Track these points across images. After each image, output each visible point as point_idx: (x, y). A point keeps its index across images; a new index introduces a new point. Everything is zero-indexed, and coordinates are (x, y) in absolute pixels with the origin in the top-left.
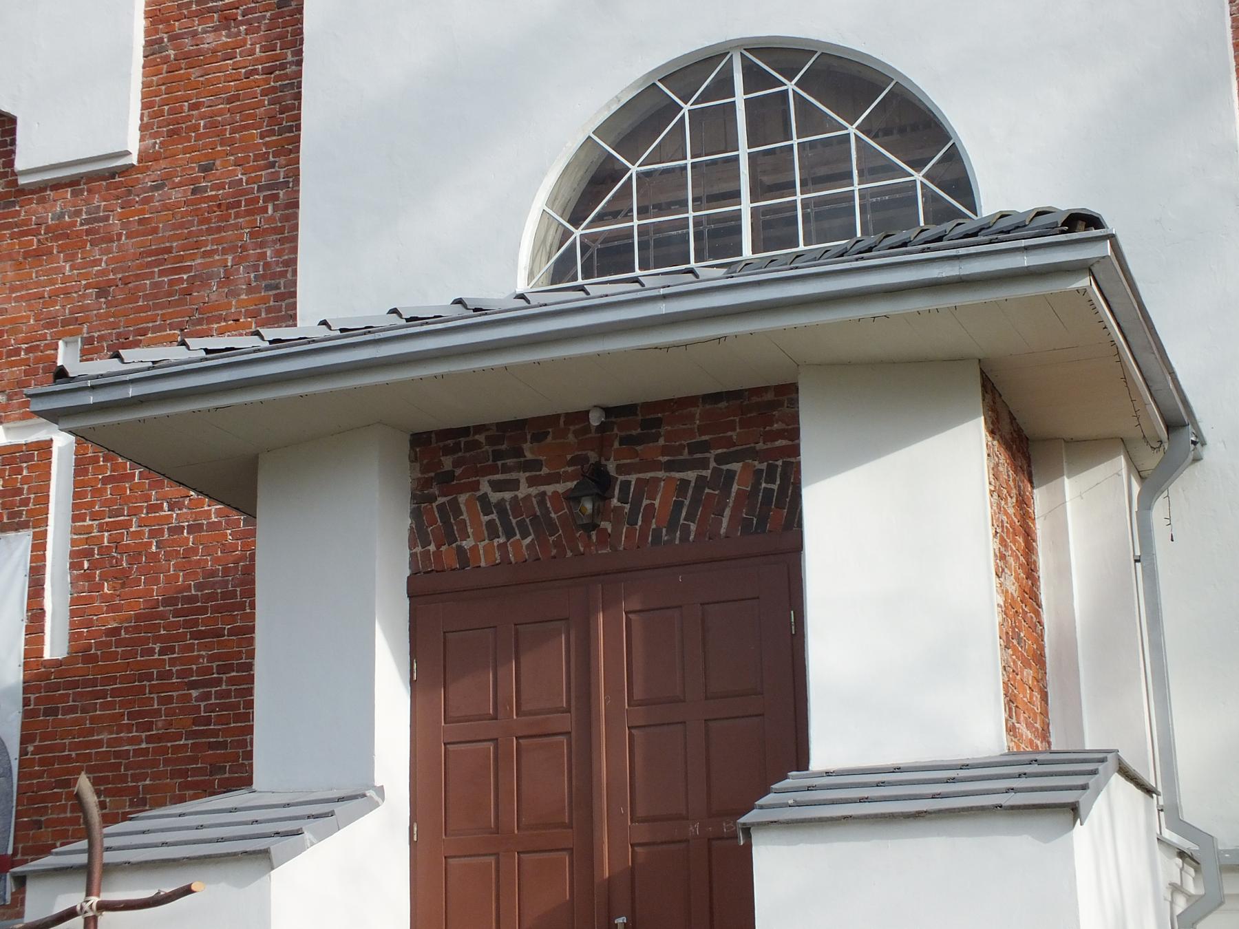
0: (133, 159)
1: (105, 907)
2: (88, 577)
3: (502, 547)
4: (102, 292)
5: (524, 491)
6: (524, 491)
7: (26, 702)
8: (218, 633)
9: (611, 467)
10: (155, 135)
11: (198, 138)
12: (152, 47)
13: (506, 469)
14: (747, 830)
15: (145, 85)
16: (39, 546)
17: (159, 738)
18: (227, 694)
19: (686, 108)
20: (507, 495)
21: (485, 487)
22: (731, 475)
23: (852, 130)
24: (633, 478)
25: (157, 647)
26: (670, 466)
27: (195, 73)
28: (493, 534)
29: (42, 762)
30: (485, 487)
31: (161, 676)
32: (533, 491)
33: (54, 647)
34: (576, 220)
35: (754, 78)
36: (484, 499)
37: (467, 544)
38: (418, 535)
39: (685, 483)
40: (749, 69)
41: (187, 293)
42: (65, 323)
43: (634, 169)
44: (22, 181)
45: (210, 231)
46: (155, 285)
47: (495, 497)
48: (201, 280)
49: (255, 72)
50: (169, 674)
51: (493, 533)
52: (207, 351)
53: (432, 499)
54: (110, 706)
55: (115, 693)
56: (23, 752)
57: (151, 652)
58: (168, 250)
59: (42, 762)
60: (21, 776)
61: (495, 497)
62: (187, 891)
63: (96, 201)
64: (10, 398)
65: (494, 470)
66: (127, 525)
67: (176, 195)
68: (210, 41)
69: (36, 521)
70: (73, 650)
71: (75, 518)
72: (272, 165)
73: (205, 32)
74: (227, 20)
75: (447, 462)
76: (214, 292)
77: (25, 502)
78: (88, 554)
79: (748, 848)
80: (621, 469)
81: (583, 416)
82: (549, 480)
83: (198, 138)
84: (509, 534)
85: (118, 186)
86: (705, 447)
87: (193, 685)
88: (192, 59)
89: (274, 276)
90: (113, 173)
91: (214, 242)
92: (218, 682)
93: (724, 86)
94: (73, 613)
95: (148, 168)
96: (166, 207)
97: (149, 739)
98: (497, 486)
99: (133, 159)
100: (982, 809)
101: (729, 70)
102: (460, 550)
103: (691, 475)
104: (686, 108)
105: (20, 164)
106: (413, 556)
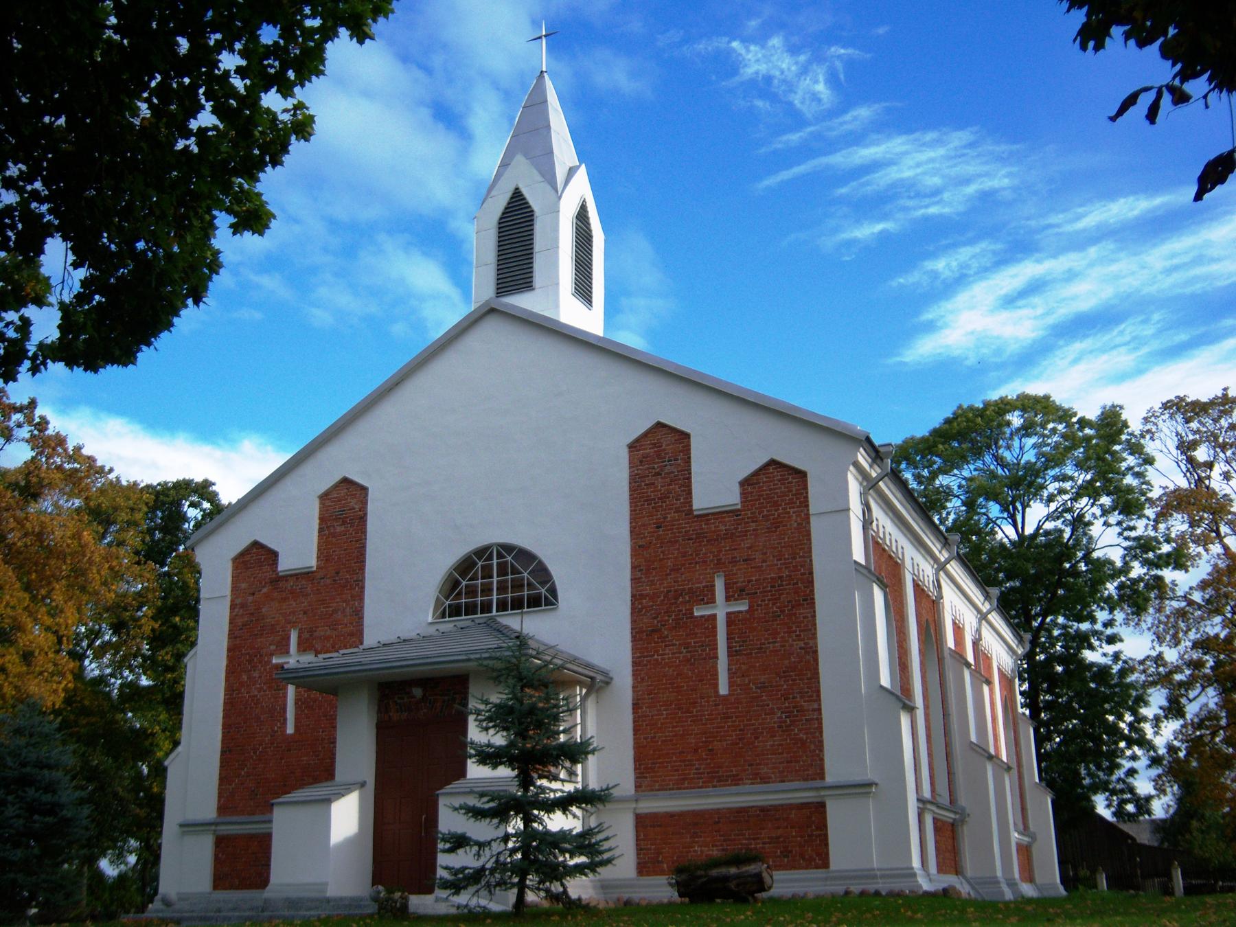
0: (315, 569)
4: (305, 613)
5: (406, 700)
6: (406, 700)
10: (322, 560)
12: (321, 530)
14: (438, 795)
15: (319, 543)
19: (480, 563)
21: (396, 699)
27: (334, 540)
34: (447, 598)
35: (500, 556)
36: (396, 702)
37: (391, 714)
38: (379, 711)
41: (332, 615)
42: (294, 622)
43: (464, 583)
46: (322, 612)
47: (399, 701)
48: (335, 611)
52: (324, 659)
61: (399, 701)
63: (304, 582)
67: (328, 581)
68: (339, 529)
74: (344, 523)
76: (339, 616)
78: (300, 700)
79: (437, 800)
85: (310, 577)
88: (333, 535)
90: (308, 573)
93: (490, 558)
98: (399, 698)
100: (459, 793)
101: (491, 553)
103: (446, 698)
104: (480, 563)
105: (280, 569)
106: (378, 717)
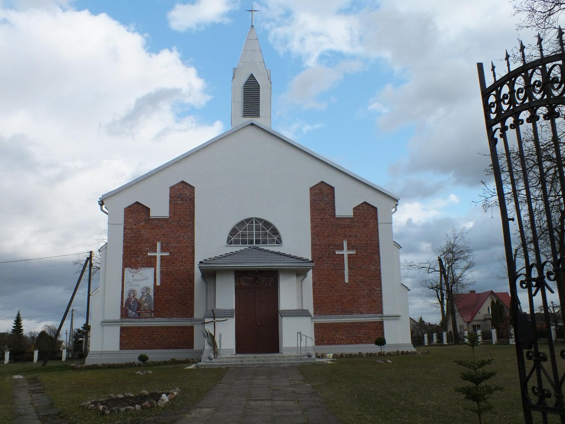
1: (216, 321)
2: (163, 275)
3: (246, 284)
7: (154, 291)
8: (183, 284)
9: (258, 277)
11: (178, 216)
13: (246, 276)
16: (155, 270)
17: (174, 297)
18: (184, 292)
20: (246, 279)
21: (243, 278)
22: (271, 279)
23: (261, 224)
24: (260, 278)
25: (174, 285)
26: (264, 278)
28: (244, 283)
29: (157, 299)
30: (243, 278)
31: (175, 289)
32: (249, 278)
33: (158, 284)
35: (256, 222)
37: (242, 283)
38: (236, 282)
39: (266, 280)
40: (255, 220)
44: (151, 218)
45: (180, 230)
47: (244, 279)
49: (187, 208)
50: (176, 289)
51: (244, 283)
53: (237, 278)
54: (167, 292)
55: (168, 291)
56: (154, 297)
57: (173, 286)
58: (174, 231)
59: (157, 299)
60: (154, 300)
61: (244, 279)
62: (227, 320)
64: (149, 249)
65: (245, 276)
66: (169, 268)
67: (175, 224)
68: (179, 202)
69: (155, 266)
70: (161, 284)
71: (161, 267)
72: (190, 222)
73: (179, 201)
75: (239, 274)
77: (153, 264)
80: (259, 277)
81: (255, 271)
82: (251, 277)
83: (178, 216)
84: (246, 283)
86: (268, 276)
87: (179, 291)
89: (190, 237)
91: (181, 231)
92: (183, 290)
94: (161, 280)
95: (170, 219)
96: (173, 225)
97: (173, 297)
98: (245, 277)
99: (168, 218)
101: (253, 220)
102: (241, 284)
